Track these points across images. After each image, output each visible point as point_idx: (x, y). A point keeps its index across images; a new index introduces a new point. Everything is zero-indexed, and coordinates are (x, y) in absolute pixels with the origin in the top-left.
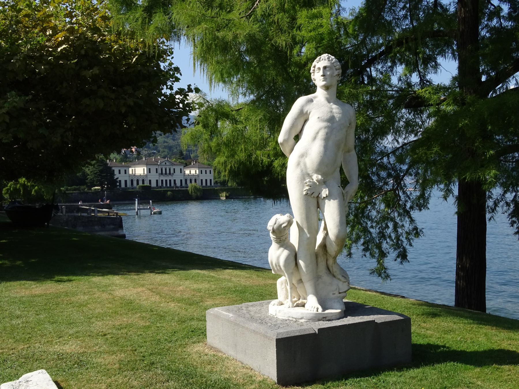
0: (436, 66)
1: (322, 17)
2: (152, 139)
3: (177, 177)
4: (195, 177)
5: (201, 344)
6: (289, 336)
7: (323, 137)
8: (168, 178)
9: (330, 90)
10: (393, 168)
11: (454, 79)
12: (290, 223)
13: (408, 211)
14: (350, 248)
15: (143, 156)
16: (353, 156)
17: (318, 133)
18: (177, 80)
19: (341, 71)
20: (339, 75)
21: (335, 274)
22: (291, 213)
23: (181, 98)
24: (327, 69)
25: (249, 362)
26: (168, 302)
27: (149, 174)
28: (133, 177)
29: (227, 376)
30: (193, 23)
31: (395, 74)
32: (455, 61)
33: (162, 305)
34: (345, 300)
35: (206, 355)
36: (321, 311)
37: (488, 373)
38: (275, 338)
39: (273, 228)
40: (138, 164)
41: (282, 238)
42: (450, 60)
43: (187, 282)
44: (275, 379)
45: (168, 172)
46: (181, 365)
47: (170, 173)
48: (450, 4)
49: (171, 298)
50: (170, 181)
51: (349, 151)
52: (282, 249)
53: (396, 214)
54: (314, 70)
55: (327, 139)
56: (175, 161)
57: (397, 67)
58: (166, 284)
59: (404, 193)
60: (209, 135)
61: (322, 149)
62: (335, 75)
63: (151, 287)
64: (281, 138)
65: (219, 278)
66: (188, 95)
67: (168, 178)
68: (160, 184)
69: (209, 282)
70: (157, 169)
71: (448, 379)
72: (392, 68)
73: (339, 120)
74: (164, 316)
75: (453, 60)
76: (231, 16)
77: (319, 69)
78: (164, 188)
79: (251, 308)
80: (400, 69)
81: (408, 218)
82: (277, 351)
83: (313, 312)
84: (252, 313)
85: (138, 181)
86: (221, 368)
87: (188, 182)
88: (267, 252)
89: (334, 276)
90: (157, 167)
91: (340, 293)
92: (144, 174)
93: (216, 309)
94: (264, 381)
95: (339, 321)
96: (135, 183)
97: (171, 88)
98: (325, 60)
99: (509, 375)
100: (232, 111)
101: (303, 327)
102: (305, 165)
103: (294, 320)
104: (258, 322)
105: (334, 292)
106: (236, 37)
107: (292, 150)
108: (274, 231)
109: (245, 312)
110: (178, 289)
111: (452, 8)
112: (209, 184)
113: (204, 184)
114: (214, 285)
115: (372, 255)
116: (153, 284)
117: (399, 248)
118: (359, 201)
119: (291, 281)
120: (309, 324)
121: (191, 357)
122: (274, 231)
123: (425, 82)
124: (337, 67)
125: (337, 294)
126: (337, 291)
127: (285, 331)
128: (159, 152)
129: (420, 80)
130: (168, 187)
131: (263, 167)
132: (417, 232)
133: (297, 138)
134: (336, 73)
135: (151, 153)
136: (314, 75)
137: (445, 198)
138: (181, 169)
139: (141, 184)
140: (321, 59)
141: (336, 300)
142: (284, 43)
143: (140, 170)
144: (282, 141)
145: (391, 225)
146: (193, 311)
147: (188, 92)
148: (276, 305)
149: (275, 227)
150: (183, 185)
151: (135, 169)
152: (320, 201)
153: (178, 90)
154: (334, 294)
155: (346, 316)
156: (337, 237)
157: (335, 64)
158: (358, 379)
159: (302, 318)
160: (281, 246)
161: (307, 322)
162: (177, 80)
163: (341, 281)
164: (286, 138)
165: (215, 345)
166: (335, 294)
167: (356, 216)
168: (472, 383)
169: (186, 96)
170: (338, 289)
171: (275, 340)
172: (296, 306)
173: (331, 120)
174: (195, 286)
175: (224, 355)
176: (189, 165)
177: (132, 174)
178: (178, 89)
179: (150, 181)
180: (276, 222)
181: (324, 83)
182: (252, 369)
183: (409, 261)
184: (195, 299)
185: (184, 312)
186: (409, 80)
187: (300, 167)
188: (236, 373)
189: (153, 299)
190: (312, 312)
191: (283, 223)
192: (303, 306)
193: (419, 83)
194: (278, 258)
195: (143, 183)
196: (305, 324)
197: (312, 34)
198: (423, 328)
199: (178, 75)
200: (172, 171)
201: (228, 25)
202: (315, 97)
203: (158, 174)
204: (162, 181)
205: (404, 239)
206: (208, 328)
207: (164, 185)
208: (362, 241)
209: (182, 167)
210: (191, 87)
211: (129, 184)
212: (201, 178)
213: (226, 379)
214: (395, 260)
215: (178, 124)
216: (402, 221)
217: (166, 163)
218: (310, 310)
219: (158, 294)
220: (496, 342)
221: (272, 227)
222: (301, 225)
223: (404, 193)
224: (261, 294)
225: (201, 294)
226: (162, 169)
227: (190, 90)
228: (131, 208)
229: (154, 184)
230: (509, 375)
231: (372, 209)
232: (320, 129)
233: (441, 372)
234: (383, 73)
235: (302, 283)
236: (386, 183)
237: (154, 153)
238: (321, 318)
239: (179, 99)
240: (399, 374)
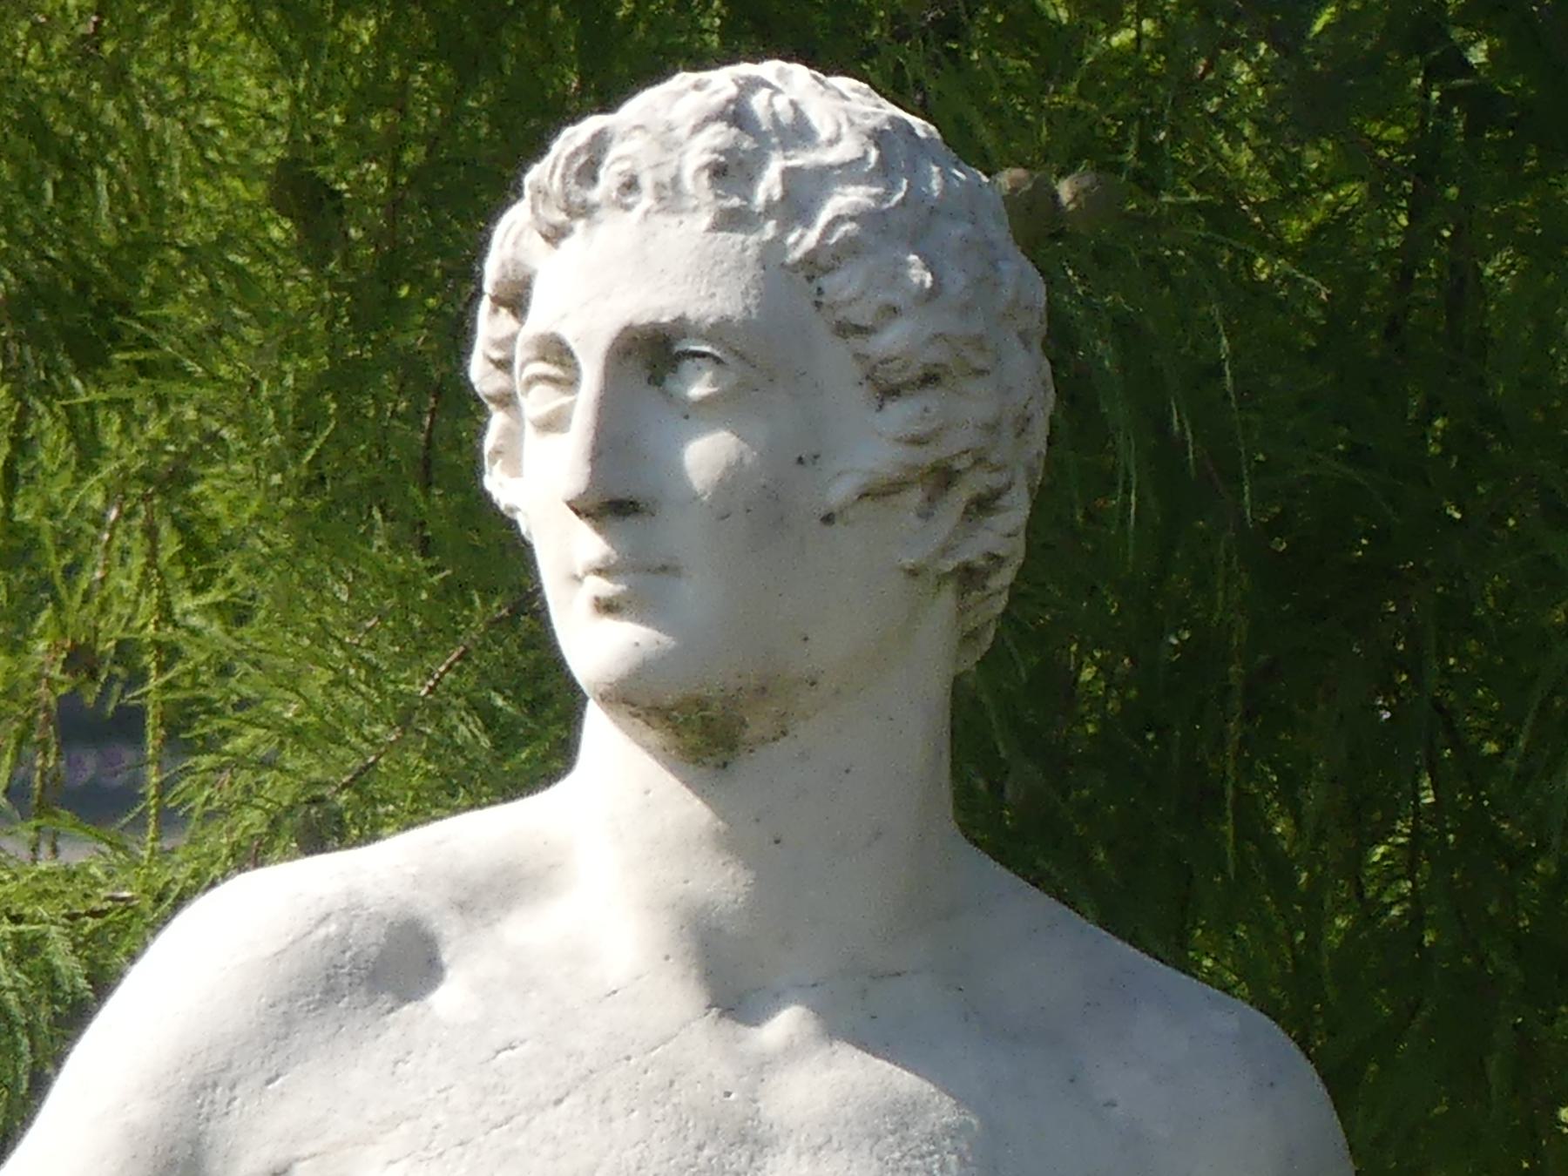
62: (840, 492)
98: (670, 195)
140: (609, 178)
157: (843, 285)
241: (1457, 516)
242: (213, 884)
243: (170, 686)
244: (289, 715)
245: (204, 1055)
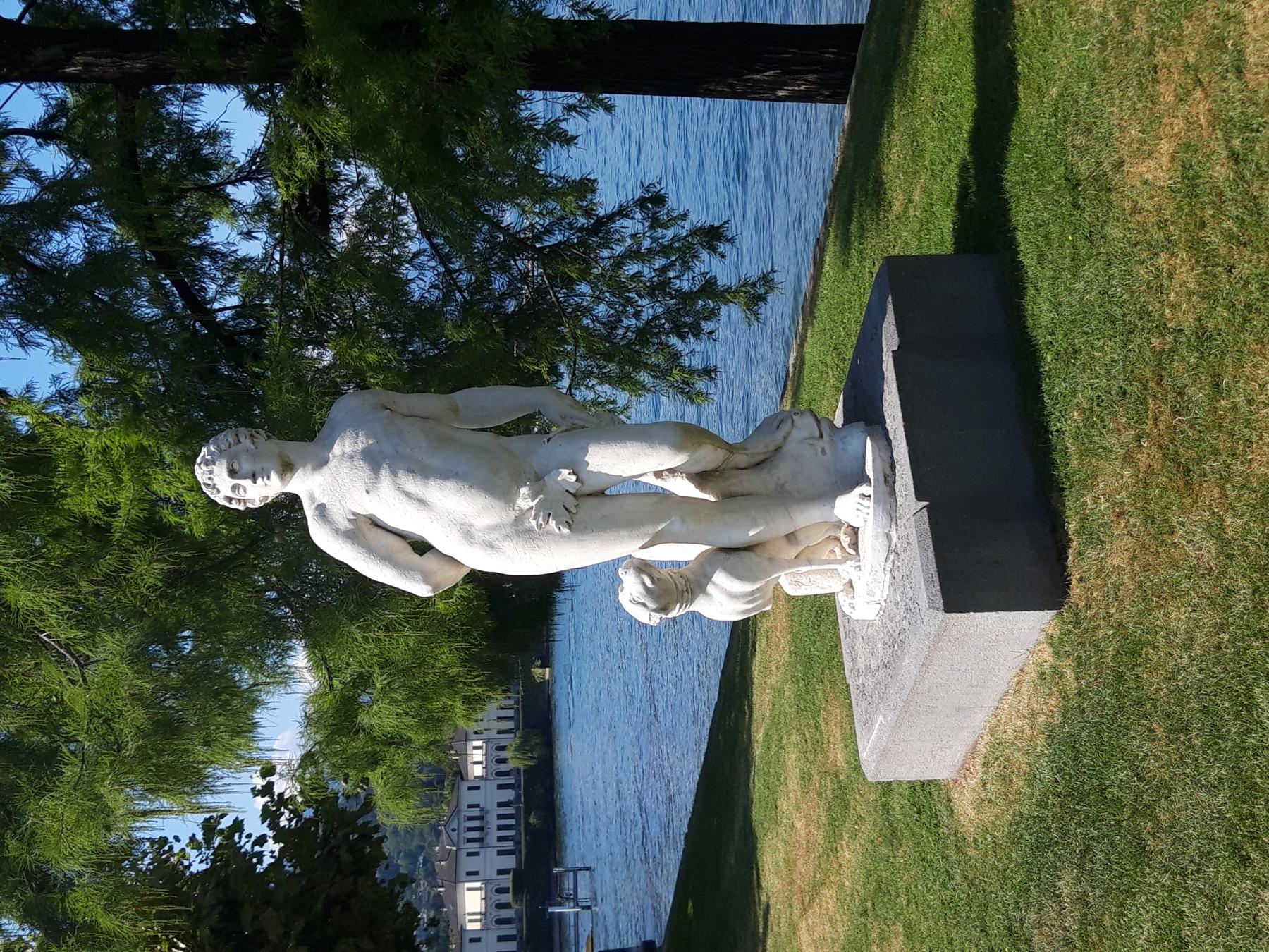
0: (213, 135)
1: (80, 448)
2: (397, 888)
3: (491, 797)
4: (490, 751)
5: (954, 795)
6: (936, 578)
7: (419, 481)
8: (494, 822)
9: (293, 458)
10: (486, 259)
11: (253, 101)
12: (643, 567)
13: (596, 221)
14: (692, 371)
15: (433, 893)
16: (469, 398)
18: (238, 825)
19: (242, 430)
20: (252, 435)
21: (772, 448)
22: (615, 564)
23: (287, 813)
24: (236, 467)
25: (1004, 676)
26: (840, 866)
27: (481, 876)
28: (490, 918)
29: (1041, 740)
30: (99, 813)
31: (233, 248)
32: (202, 95)
33: (847, 883)
34: (839, 420)
35: (984, 784)
36: (868, 488)
37: (1028, 65)
38: (941, 615)
39: (655, 610)
40: (455, 904)
42: (201, 108)
43: (783, 805)
44: (1048, 615)
45: (476, 824)
46: (1014, 855)
47: (481, 818)
48: (46, 96)
49: (828, 855)
50: (500, 817)
51: (455, 410)
52: (710, 588)
53: (605, 253)
54: (239, 500)
55: (425, 472)
56: (448, 805)
57: (214, 240)
58: (790, 864)
59: (549, 231)
60: (397, 748)
61: (450, 484)
62: (253, 447)
63: (796, 903)
64: (421, 590)
65: (772, 717)
66: (281, 795)
67: (494, 822)
68: (509, 845)
69: (782, 748)
70: (469, 854)
71: (1045, 169)
72: (215, 256)
73: (374, 436)
74: (879, 880)
75: (201, 101)
76: (80, 708)
77: (235, 488)
78: (519, 833)
79: (861, 663)
80: (221, 232)
81: (614, 222)
82: (975, 611)
83: (872, 508)
84: (874, 663)
85: (500, 906)
86: (1018, 750)
87: (503, 767)
89: (778, 449)
90: (464, 852)
92: (480, 889)
93: (863, 755)
94: (1055, 644)
95: (894, 443)
96: (506, 914)
97: (261, 840)
98: (211, 472)
99: (1033, 14)
100: (332, 688)
101: (913, 538)
102: (493, 528)
103: (892, 557)
104: (899, 653)
105: (819, 450)
106: (136, 698)
107: (452, 560)
108: (664, 609)
109: (870, 681)
110: (803, 833)
111: (55, 91)
112: (511, 713)
113: (510, 725)
114: (789, 734)
115: (713, 315)
116: (789, 898)
117: (690, 247)
118: (569, 348)
119: (789, 564)
120: (904, 521)
121: (989, 825)
122: (664, 609)
123: (254, 167)
124: (231, 440)
125: (825, 443)
126: (815, 442)
127: (923, 587)
128: (422, 848)
129: (250, 180)
130: (518, 824)
131: (478, 597)
132: (652, 201)
133: (422, 547)
134: (246, 443)
135: (426, 870)
136: (253, 501)
137: (568, 140)
138: (470, 788)
139: (507, 898)
140: (209, 482)
141: (841, 446)
142: (155, 565)
143: (472, 900)
144: (429, 588)
145: (632, 268)
146: (862, 805)
147: (272, 795)
149: (651, 605)
150: (513, 782)
151: (470, 914)
153: (266, 824)
155: (881, 422)
156: (679, 447)
157: (223, 447)
158: (1046, 399)
159: (888, 537)
160: (702, 590)
161: (897, 525)
162: (238, 825)
163: (789, 433)
164: (419, 577)
166: (823, 449)
167: (609, 357)
168: (1056, 110)
169: (282, 801)
170: (811, 442)
171: (948, 615)
172: (856, 549)
173: (374, 460)
174: (794, 785)
175: (985, 737)
176: (458, 766)
177: (480, 920)
178: (263, 822)
179: (500, 872)
180: (639, 603)
181: (273, 476)
182: (1021, 670)
183: (727, 222)
184: (829, 792)
185: (868, 828)
186: (249, 210)
188: (1033, 715)
189: (831, 904)
190: (871, 511)
191: (644, 584)
192: (855, 531)
193: (257, 185)
194: (733, 596)
195: (505, 891)
196: (902, 531)
197: (126, 477)
198: (906, 209)
199: (226, 823)
200: (476, 812)
201: (104, 719)
202: (312, 499)
203: (482, 851)
204: (500, 839)
205: (670, 233)
206: (913, 777)
207: (512, 833)
208: (674, 340)
209: (465, 785)
210: (259, 787)
211: (510, 930)
212: (494, 734)
213: (1049, 741)
214: (723, 256)
215: (360, 821)
216: (623, 240)
217: (454, 830)
218: (865, 516)
219: (816, 887)
220: (944, 29)
222: (646, 541)
223: (549, 231)
224: (813, 614)
225: (814, 772)
226: (470, 840)
227: (267, 790)
228: (572, 923)
229: (510, 862)
230: (1033, 14)
231: (591, 315)
232: (398, 488)
233: (1025, 183)
234: (229, 277)
235: (797, 534)
236: (525, 276)
237: (425, 863)
239: (290, 820)
240: (1031, 292)
241: (251, 21)
242: (909, 782)
243: (78, 456)
244: (788, 408)
245: (987, 738)
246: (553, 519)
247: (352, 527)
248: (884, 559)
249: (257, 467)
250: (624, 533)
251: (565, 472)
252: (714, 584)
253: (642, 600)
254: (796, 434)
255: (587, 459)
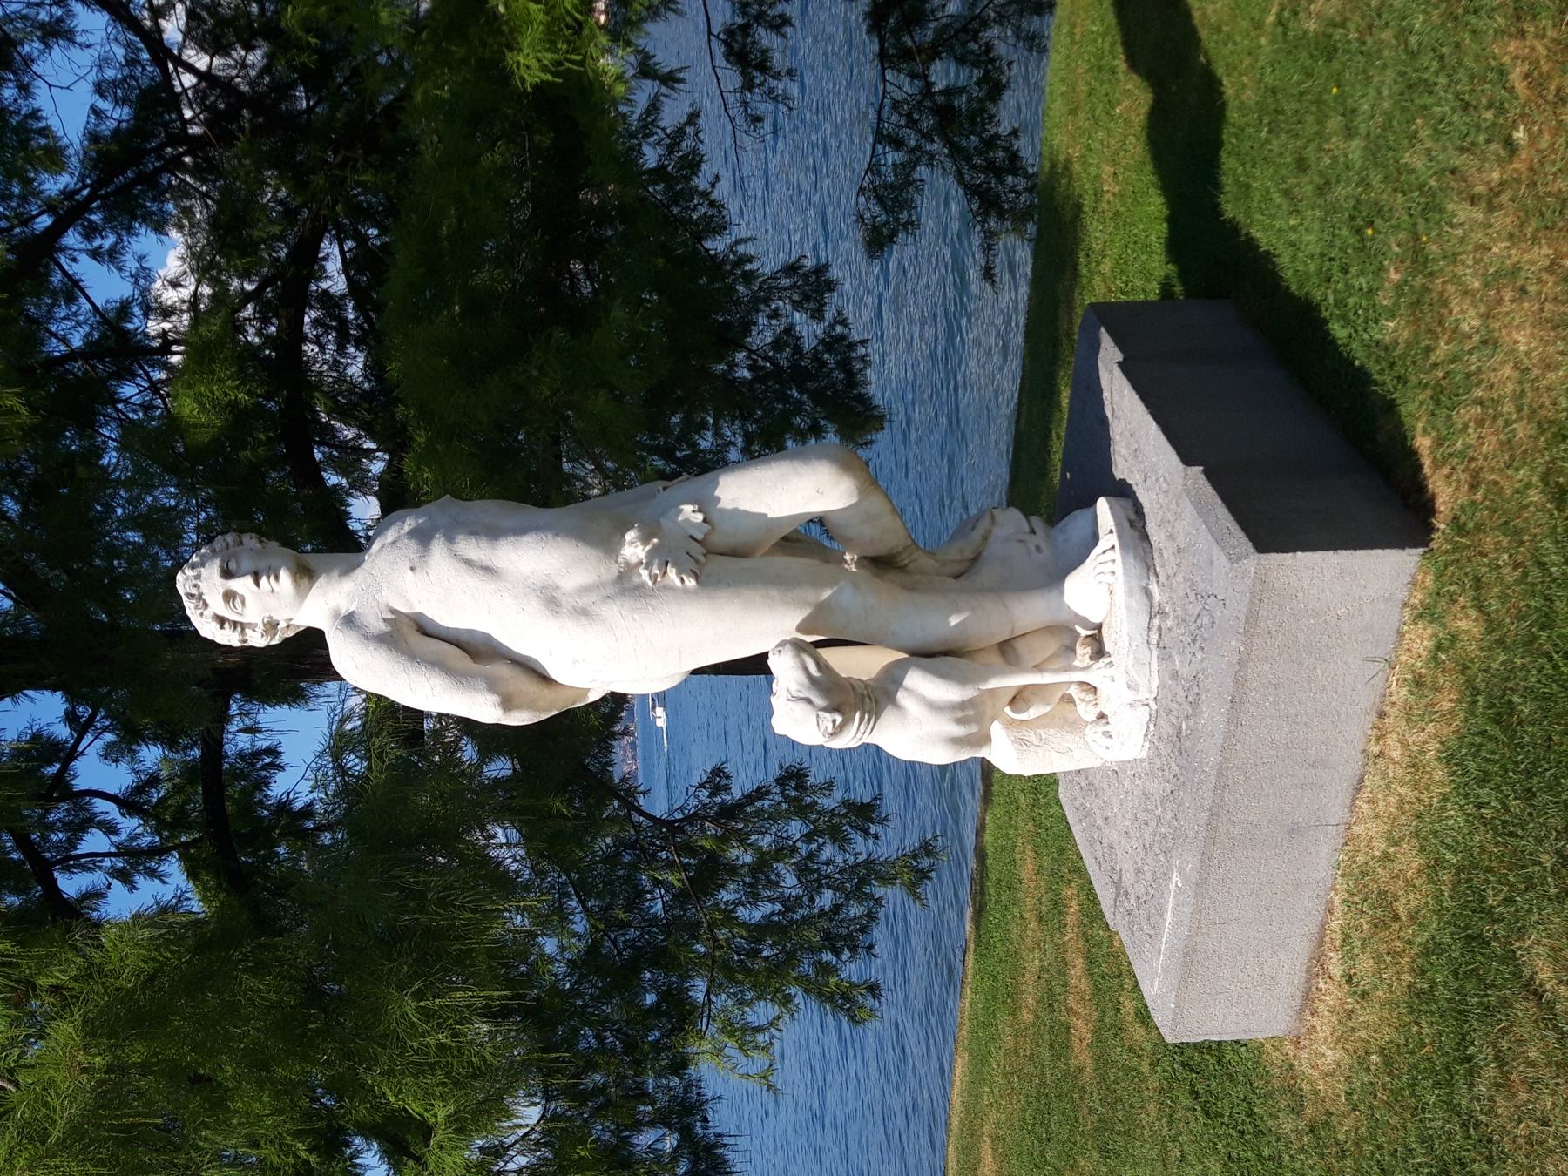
7: (484, 543)
17: (469, 563)
21: (968, 554)
25: (1355, 734)
39: (825, 709)
41: (859, 691)
52: (901, 696)
61: (528, 539)
88: (912, 767)
89: (976, 559)
91: (1033, 532)
93: (1151, 990)
102: (586, 590)
103: (1156, 622)
105: (1033, 548)
140: (194, 591)
148: (1106, 728)
149: (819, 701)
152: (717, 540)
154: (1038, 548)
159: (1147, 593)
160: (890, 698)
163: (989, 532)
165: (1299, 978)
180: (801, 699)
181: (285, 576)
187: (594, 608)
190: (1118, 566)
194: (935, 707)
218: (1110, 578)
221: (821, 713)
238: (1136, 534)
246: (673, 566)
247: (389, 629)
248: (1146, 626)
249: (262, 565)
250: (774, 593)
251: (688, 509)
252: (907, 689)
253: (805, 694)
254: (998, 532)
255: (717, 493)
